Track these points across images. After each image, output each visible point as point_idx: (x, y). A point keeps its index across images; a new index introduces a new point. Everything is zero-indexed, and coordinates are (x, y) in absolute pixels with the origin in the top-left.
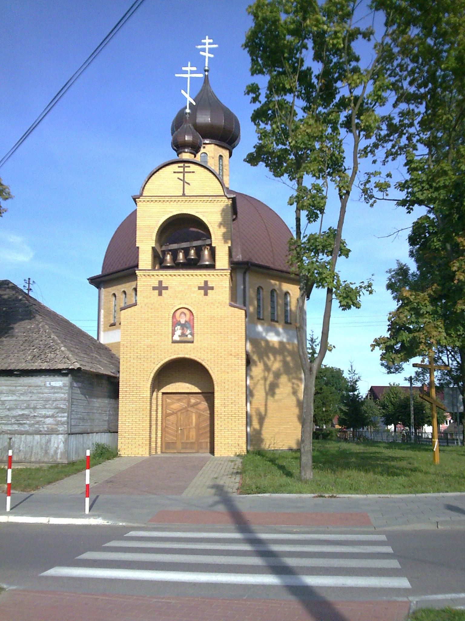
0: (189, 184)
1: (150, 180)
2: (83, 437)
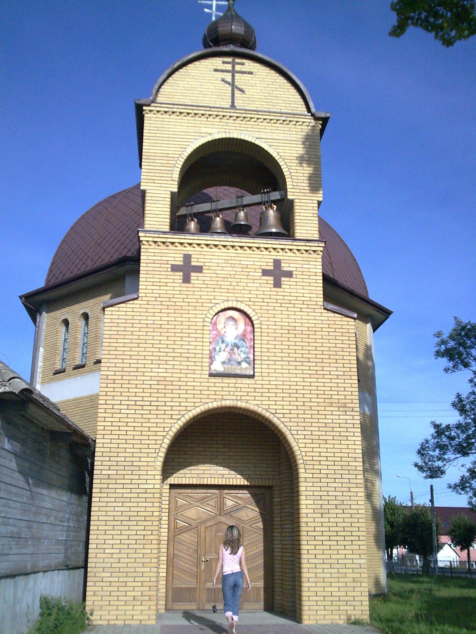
0: (242, 91)
1: (171, 78)
2: (15, 584)
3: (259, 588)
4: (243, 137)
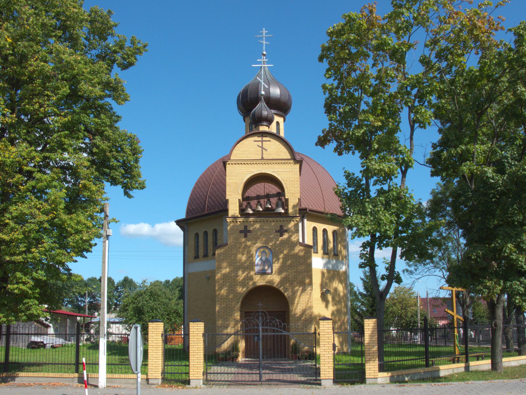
0: (266, 150)
3: (285, 292)
4: (267, 172)
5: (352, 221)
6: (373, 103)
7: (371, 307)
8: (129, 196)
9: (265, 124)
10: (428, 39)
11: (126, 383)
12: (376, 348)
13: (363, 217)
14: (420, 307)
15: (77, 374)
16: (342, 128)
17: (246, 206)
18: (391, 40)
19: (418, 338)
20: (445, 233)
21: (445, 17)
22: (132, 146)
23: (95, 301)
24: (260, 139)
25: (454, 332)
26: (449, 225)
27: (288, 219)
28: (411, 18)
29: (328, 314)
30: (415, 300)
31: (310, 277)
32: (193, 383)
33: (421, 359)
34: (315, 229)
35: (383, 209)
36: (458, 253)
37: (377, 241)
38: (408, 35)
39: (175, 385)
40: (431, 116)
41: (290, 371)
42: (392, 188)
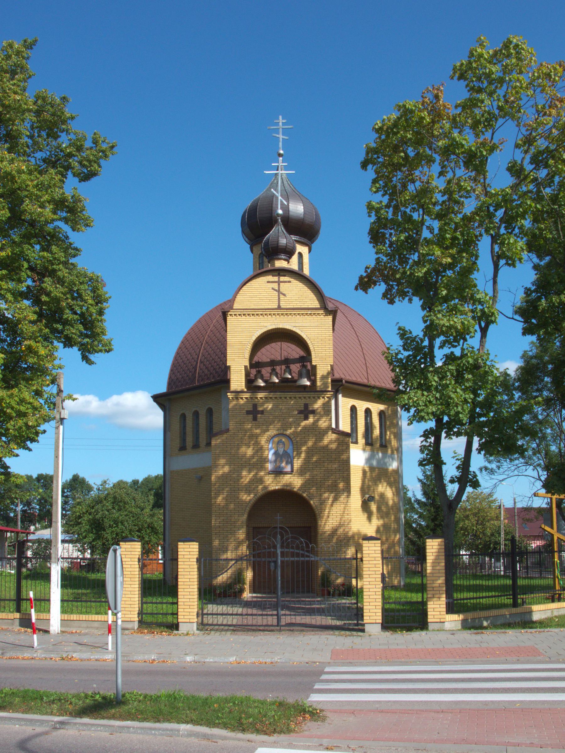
0: (284, 295)
5: (409, 398)
6: (440, 229)
7: (433, 520)
8: (89, 362)
9: (283, 257)
10: (520, 136)
11: (87, 627)
12: (441, 581)
13: (425, 393)
14: (504, 520)
15: (18, 614)
16: (395, 266)
17: (255, 375)
18: (465, 140)
19: (500, 567)
20: (542, 414)
21: (544, 105)
22: (95, 292)
23: (30, 509)
24: (276, 279)
25: (554, 558)
26: (548, 402)
27: (316, 395)
28: (495, 107)
29: (370, 530)
30: (497, 511)
31: (347, 480)
32: (183, 628)
33: (507, 595)
34: (353, 409)
35: (453, 382)
36: (560, 444)
37: (445, 428)
38: (490, 131)
39: (158, 630)
40: (523, 249)
41: (320, 612)
42: (466, 352)
